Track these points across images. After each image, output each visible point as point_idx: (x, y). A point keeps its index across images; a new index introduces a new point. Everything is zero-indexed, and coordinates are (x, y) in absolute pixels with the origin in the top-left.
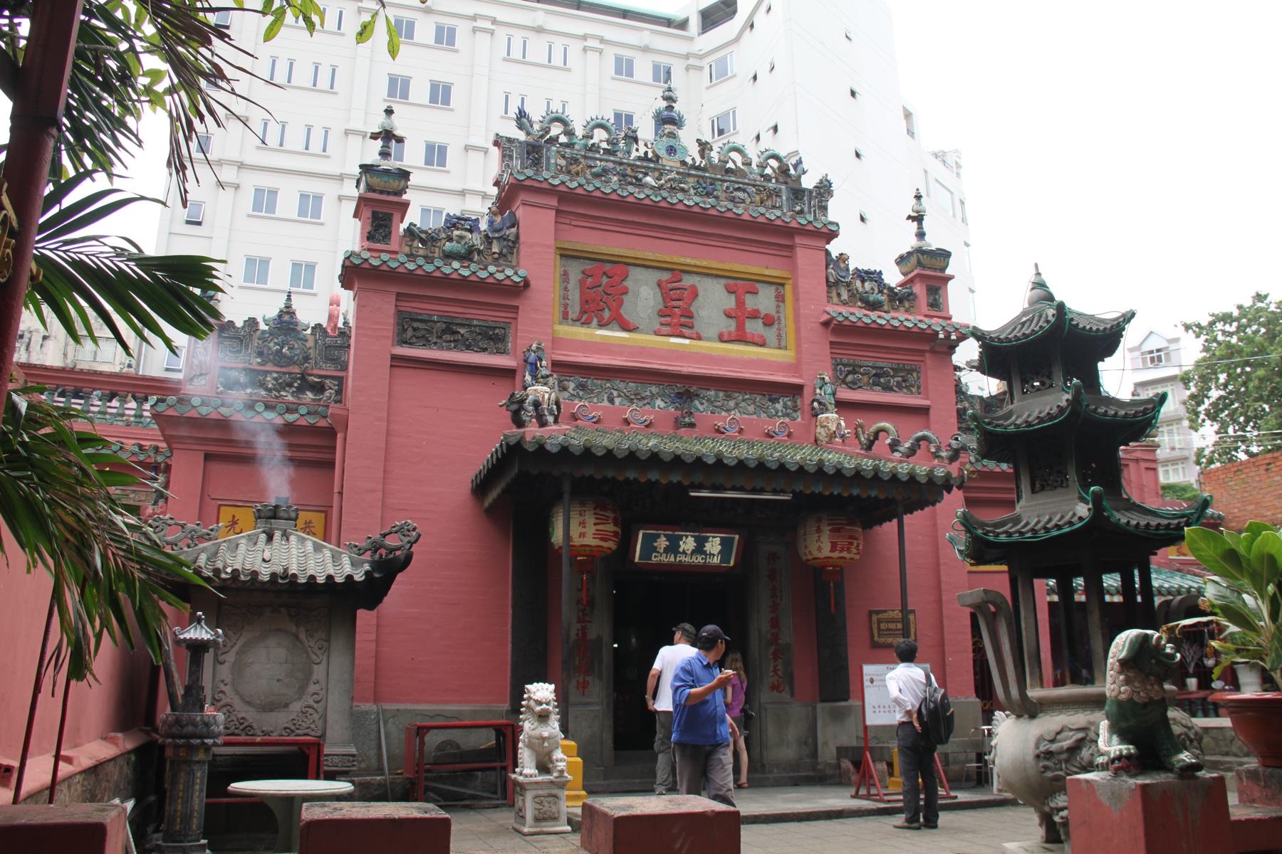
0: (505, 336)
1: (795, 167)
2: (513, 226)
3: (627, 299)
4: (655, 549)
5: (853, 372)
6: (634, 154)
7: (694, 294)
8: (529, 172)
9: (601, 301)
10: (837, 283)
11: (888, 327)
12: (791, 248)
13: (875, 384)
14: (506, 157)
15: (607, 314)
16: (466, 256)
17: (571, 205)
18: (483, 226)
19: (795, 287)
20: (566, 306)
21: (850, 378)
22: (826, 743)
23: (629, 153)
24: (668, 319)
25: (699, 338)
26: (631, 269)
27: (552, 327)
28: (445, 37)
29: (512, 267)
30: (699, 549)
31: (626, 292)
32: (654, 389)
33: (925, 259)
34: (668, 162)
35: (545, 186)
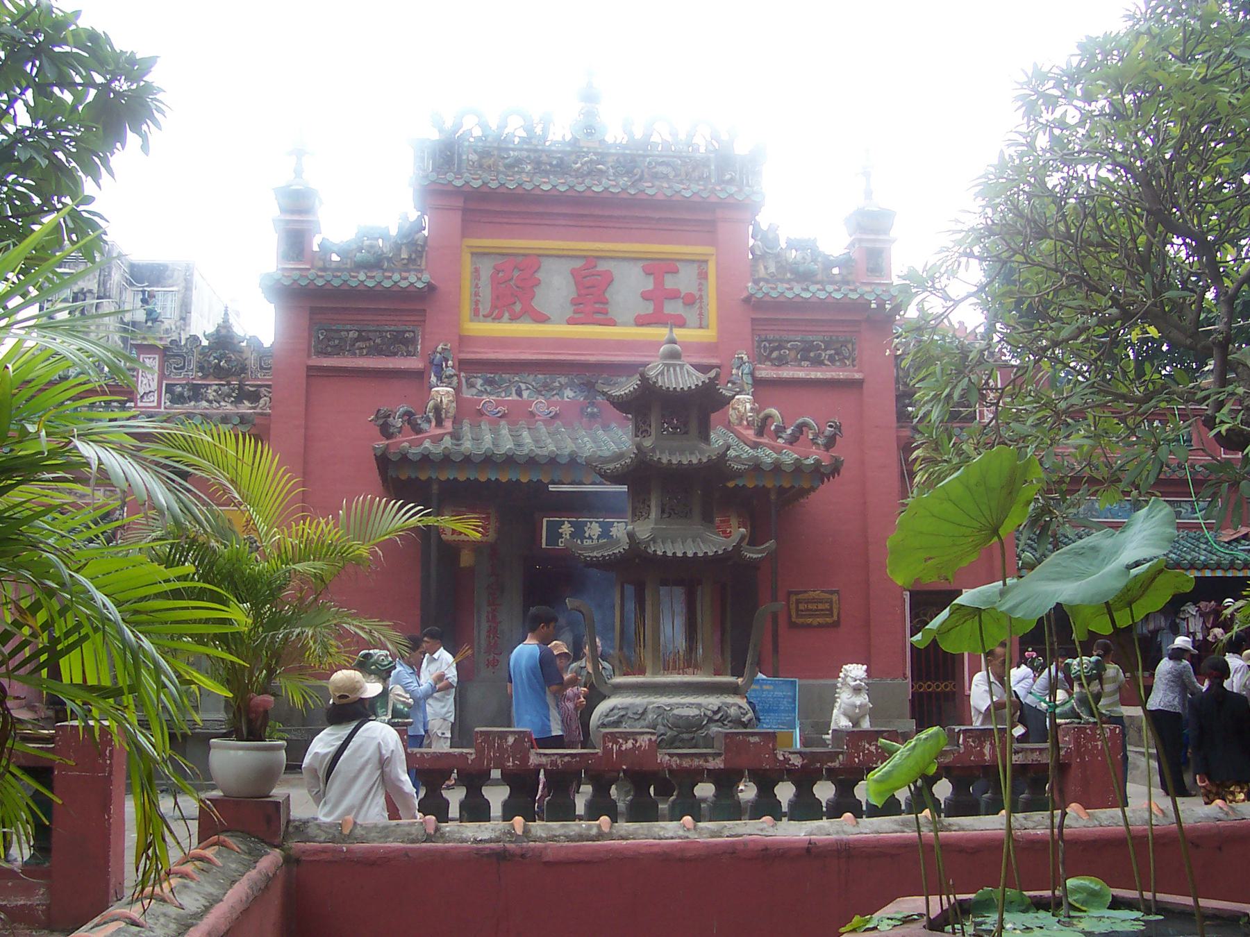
3: (539, 292)
5: (779, 348)
13: (804, 359)
15: (518, 307)
20: (477, 302)
21: (775, 354)
31: (538, 283)
32: (563, 380)
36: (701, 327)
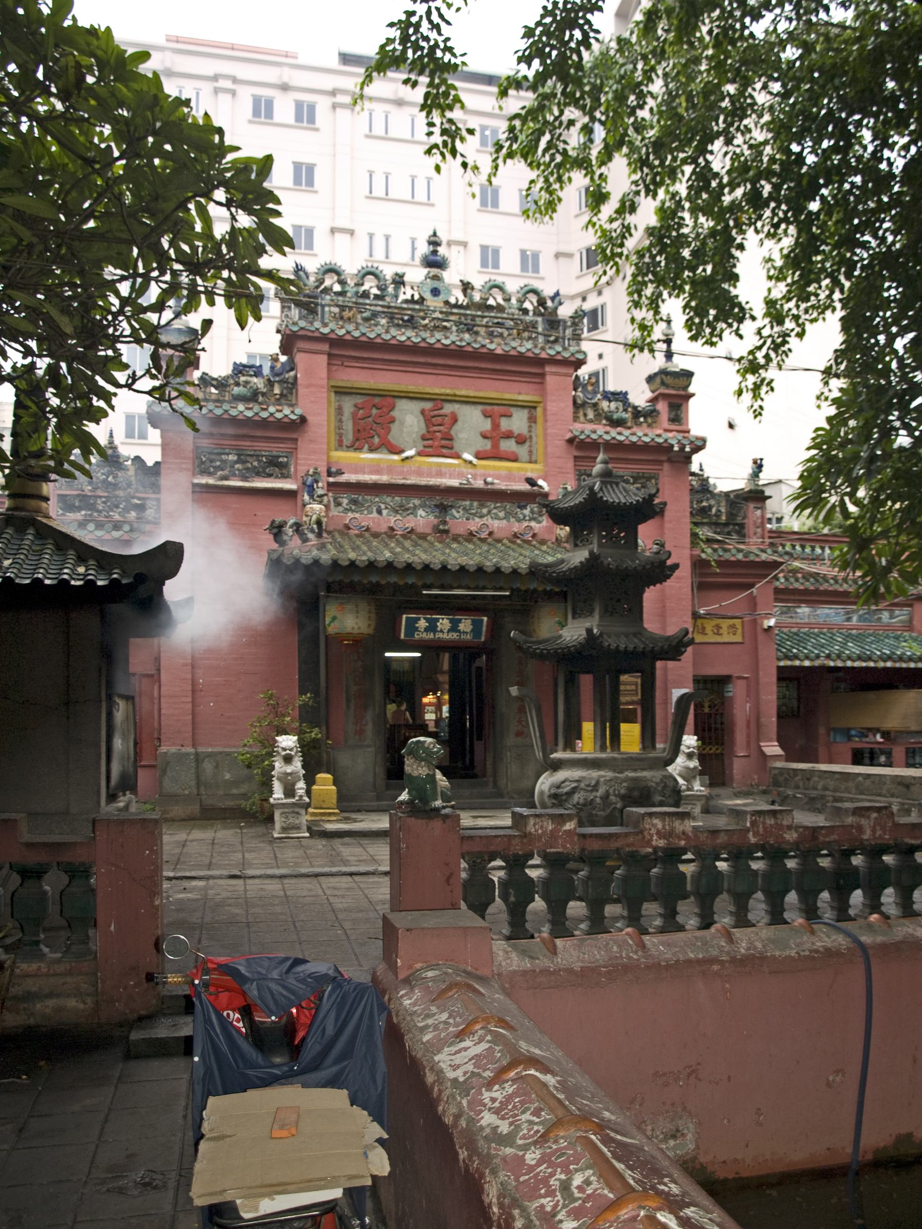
0: (287, 463)
1: (553, 299)
2: (292, 369)
3: (395, 427)
4: (417, 629)
6: (402, 297)
7: (454, 419)
8: (302, 324)
9: (371, 429)
10: (584, 404)
11: (627, 442)
12: (543, 375)
15: (376, 440)
16: (253, 397)
17: (340, 349)
18: (266, 371)
19: (545, 410)
20: (341, 435)
23: (397, 297)
24: (430, 442)
28: (305, 115)
29: (291, 405)
30: (454, 628)
31: (393, 421)
32: (417, 502)
34: (433, 303)
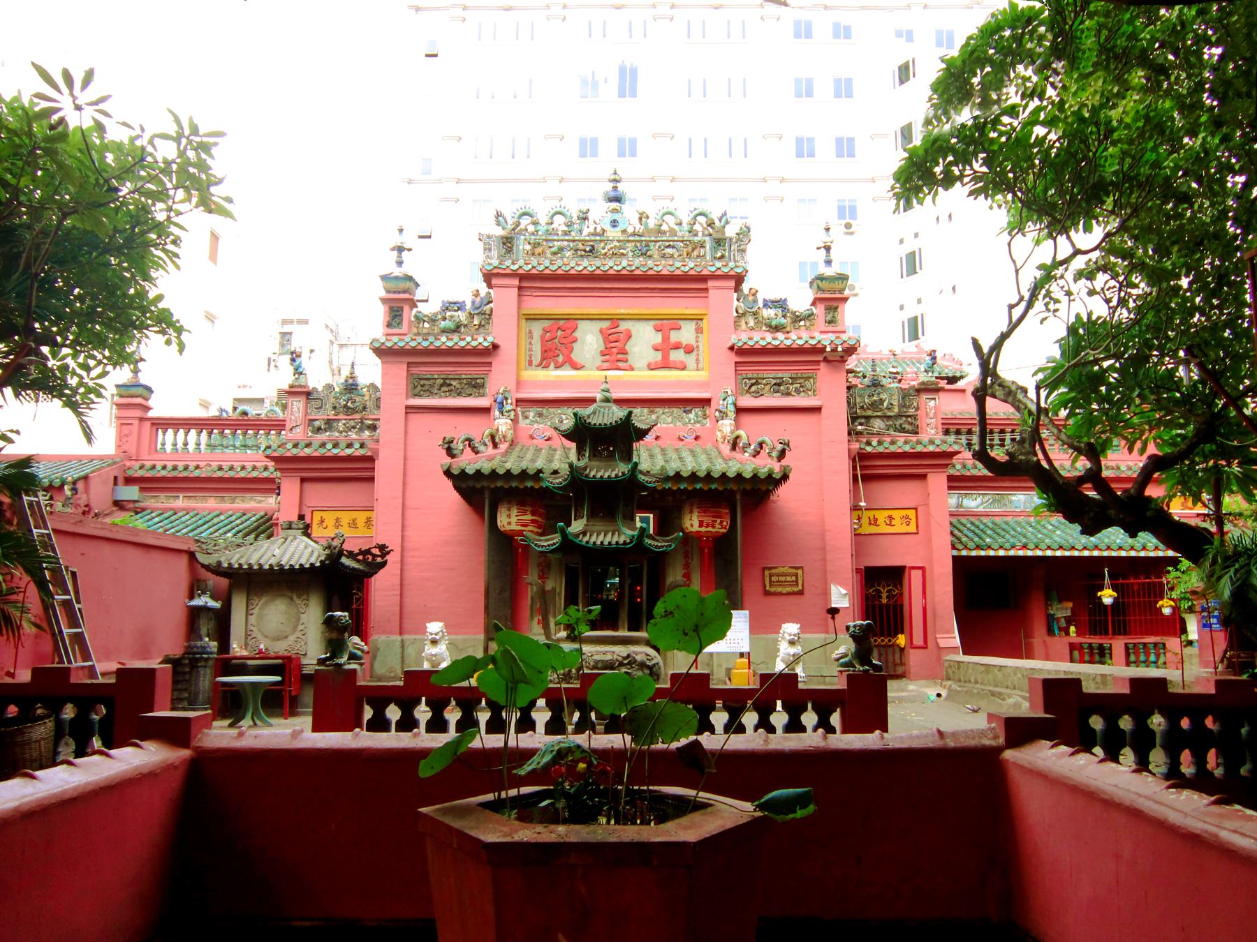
5: (757, 383)
14: (488, 249)
15: (560, 359)
17: (528, 281)
18: (469, 306)
20: (530, 356)
21: (754, 388)
22: (720, 666)
23: (581, 231)
25: (632, 369)
26: (579, 322)
27: (520, 372)
31: (575, 340)
33: (823, 285)
35: (508, 271)
36: (698, 370)
